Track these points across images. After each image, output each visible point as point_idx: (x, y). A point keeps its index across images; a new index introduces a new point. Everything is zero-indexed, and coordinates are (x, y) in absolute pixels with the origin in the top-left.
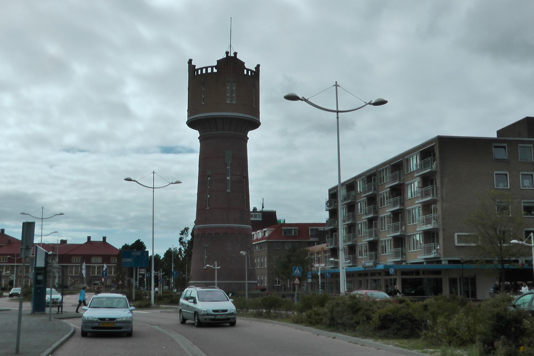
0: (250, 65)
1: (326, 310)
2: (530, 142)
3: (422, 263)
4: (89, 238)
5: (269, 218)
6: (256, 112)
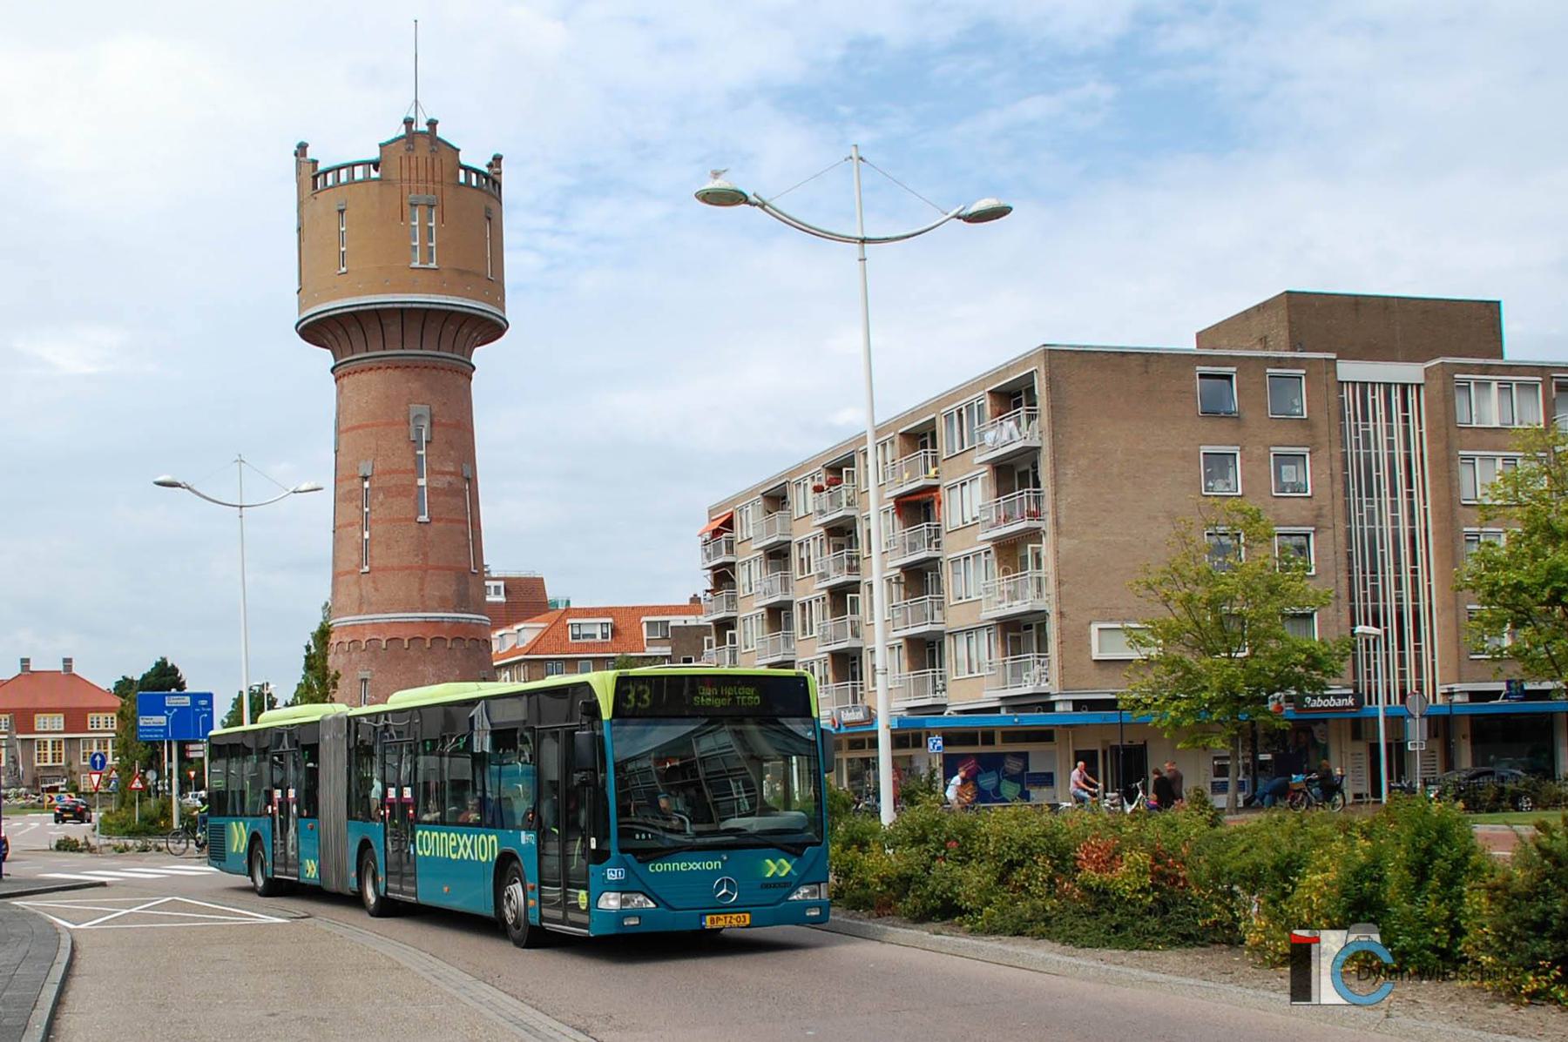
0: (475, 157)
1: (1435, 807)
2: (1296, 363)
3: (996, 710)
4: (25, 662)
5: (526, 597)
6: (494, 287)
